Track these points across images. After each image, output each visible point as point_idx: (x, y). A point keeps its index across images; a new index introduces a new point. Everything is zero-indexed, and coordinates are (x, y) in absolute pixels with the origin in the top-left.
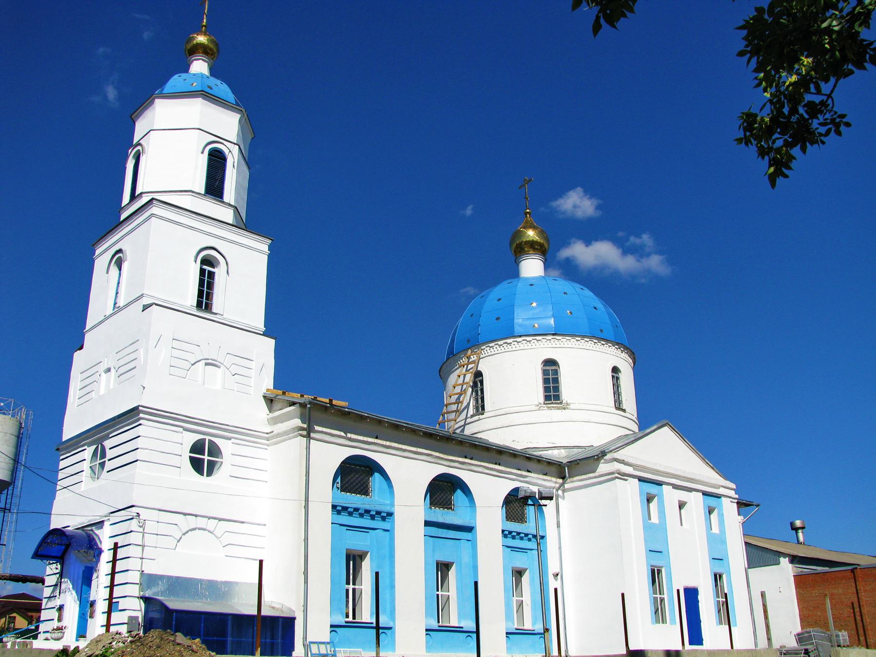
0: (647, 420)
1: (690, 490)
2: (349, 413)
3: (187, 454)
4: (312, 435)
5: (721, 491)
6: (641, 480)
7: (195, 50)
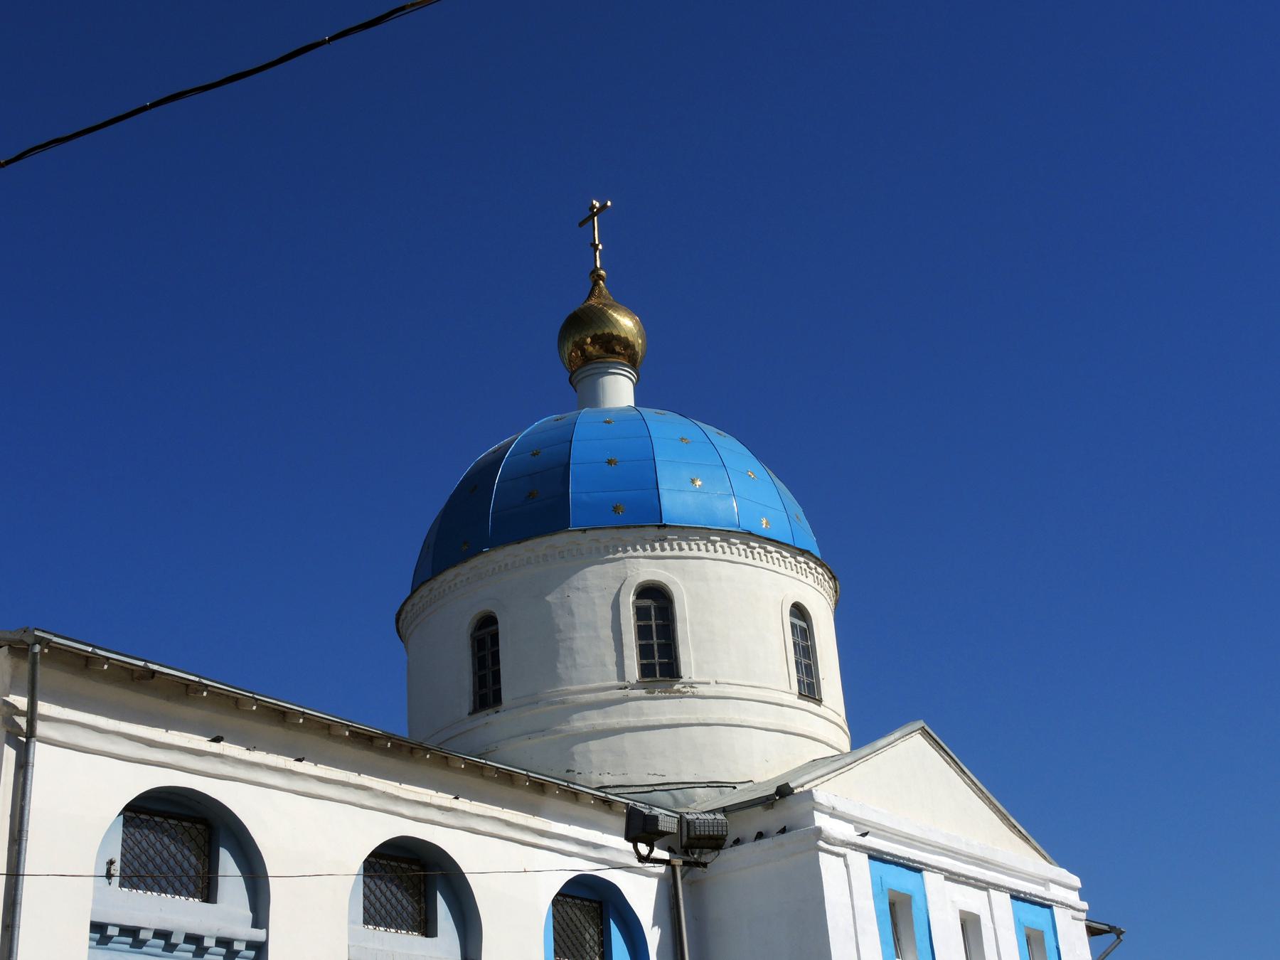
0: (867, 726)
1: (985, 886)
5: (1055, 893)
7: (615, 349)
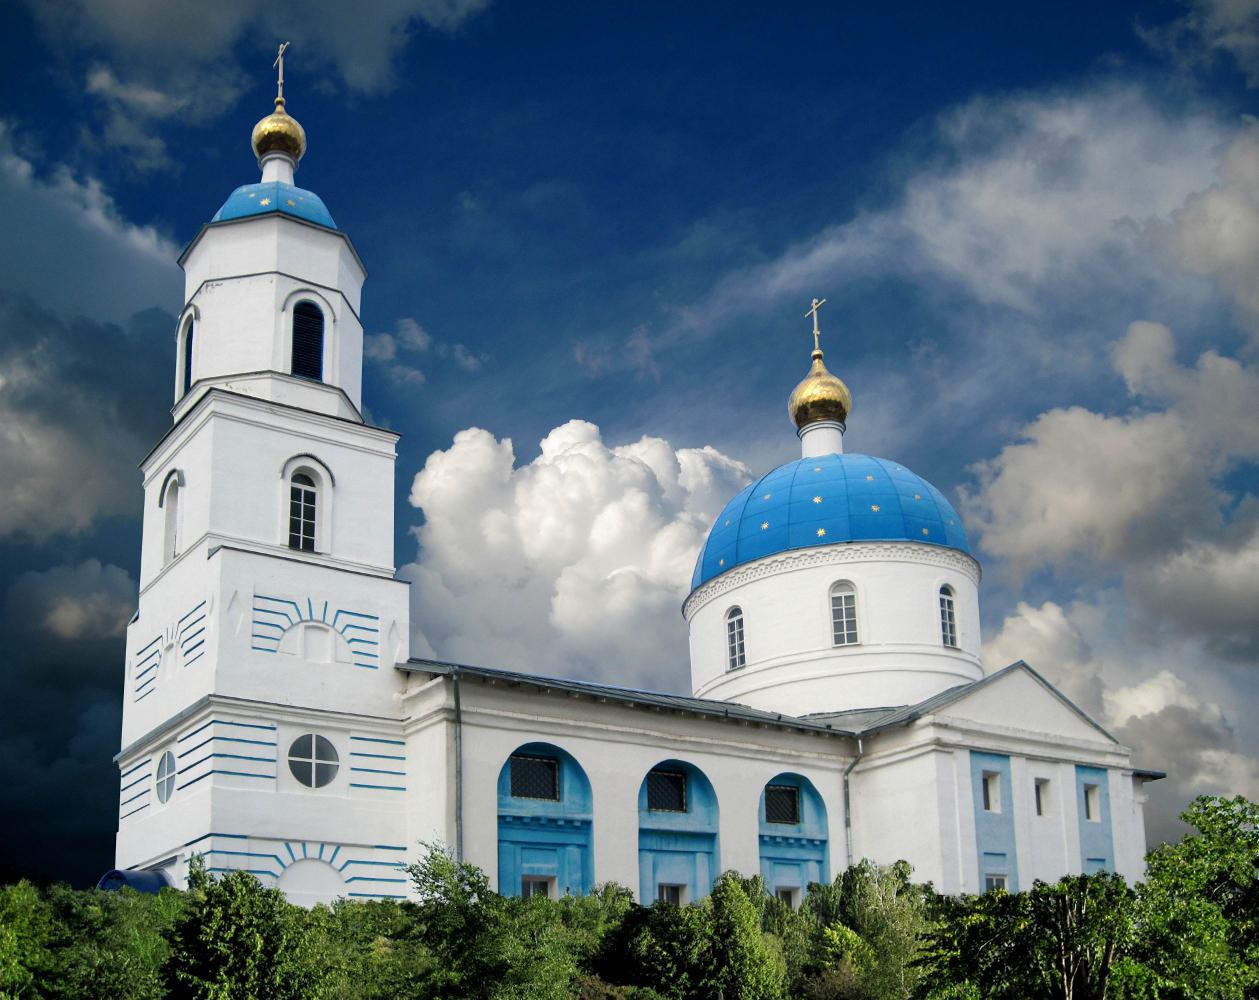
1: (1056, 761)
2: (519, 683)
3: (285, 759)
4: (464, 718)
6: (975, 752)
